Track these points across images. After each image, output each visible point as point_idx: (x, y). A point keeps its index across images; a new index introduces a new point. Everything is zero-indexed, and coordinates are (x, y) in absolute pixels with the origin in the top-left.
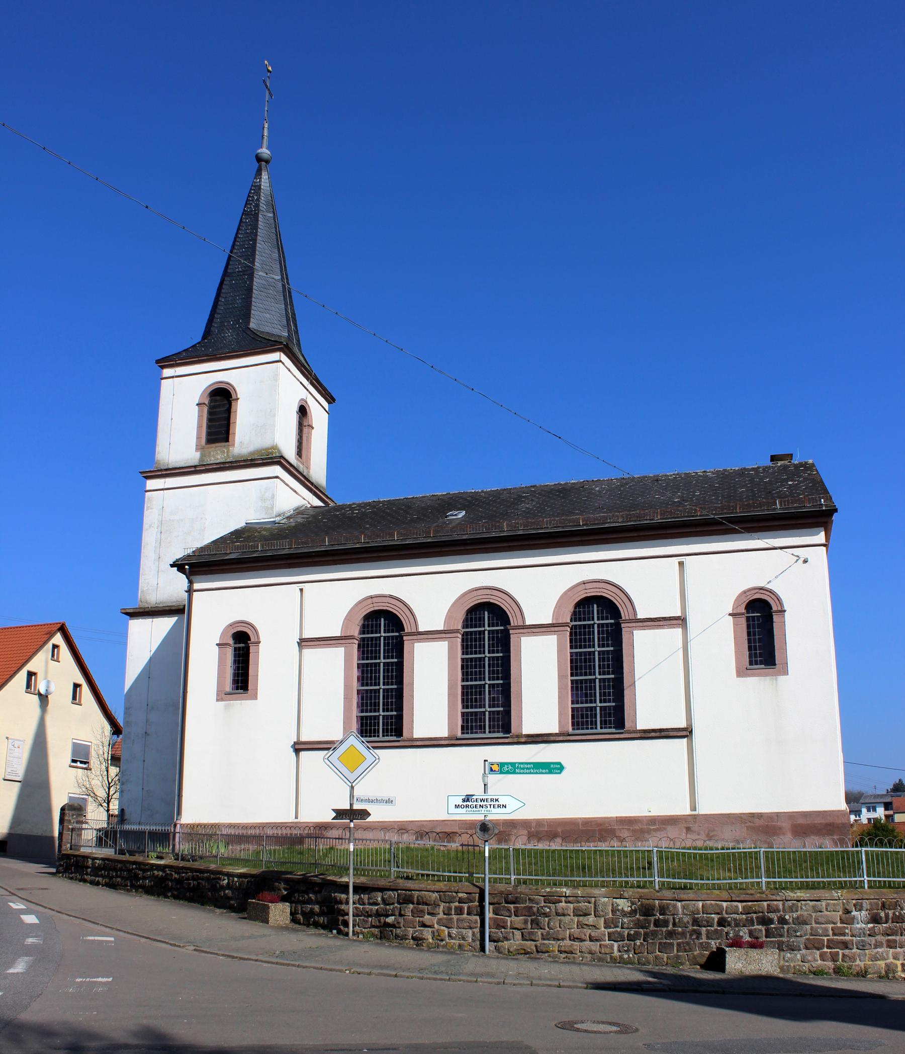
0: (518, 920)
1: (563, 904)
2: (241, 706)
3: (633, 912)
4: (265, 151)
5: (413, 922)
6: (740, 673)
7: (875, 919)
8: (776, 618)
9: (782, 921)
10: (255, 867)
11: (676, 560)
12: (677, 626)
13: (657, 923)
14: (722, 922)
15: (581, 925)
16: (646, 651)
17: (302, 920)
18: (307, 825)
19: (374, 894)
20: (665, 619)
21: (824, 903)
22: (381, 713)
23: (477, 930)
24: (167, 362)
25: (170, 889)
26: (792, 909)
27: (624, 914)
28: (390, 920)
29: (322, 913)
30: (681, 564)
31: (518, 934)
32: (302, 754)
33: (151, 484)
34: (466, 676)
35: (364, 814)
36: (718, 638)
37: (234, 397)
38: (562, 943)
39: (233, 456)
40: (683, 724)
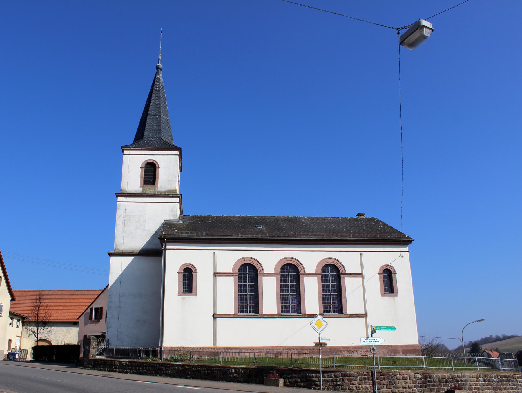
0: (385, 382)
1: (398, 376)
2: (189, 298)
3: (421, 378)
4: (160, 65)
5: (348, 383)
6: (382, 295)
7: (485, 381)
8: (393, 276)
9: (462, 381)
10: (248, 365)
11: (359, 253)
12: (360, 277)
13: (429, 382)
14: (447, 381)
15: (405, 383)
16: (350, 286)
17: (290, 384)
18: (220, 348)
19: (330, 374)
20: (356, 274)
21: (471, 375)
22: (248, 304)
23: (371, 386)
24: (123, 148)
25: (189, 375)
26: (464, 377)
27: (419, 379)
28: (339, 383)
29: (301, 382)
30: (361, 254)
31: (385, 386)
32: (217, 319)
33: (120, 199)
34: (282, 291)
35: (325, 344)
36: (375, 283)
37: (157, 167)
38: (400, 389)
39: (158, 192)
40: (363, 313)
